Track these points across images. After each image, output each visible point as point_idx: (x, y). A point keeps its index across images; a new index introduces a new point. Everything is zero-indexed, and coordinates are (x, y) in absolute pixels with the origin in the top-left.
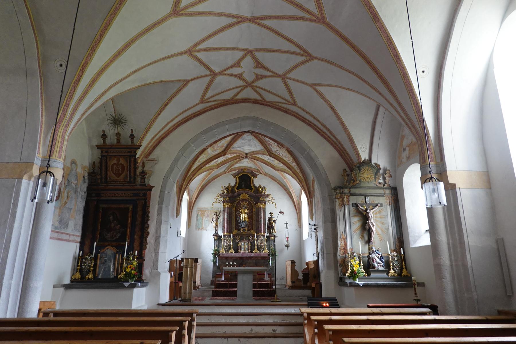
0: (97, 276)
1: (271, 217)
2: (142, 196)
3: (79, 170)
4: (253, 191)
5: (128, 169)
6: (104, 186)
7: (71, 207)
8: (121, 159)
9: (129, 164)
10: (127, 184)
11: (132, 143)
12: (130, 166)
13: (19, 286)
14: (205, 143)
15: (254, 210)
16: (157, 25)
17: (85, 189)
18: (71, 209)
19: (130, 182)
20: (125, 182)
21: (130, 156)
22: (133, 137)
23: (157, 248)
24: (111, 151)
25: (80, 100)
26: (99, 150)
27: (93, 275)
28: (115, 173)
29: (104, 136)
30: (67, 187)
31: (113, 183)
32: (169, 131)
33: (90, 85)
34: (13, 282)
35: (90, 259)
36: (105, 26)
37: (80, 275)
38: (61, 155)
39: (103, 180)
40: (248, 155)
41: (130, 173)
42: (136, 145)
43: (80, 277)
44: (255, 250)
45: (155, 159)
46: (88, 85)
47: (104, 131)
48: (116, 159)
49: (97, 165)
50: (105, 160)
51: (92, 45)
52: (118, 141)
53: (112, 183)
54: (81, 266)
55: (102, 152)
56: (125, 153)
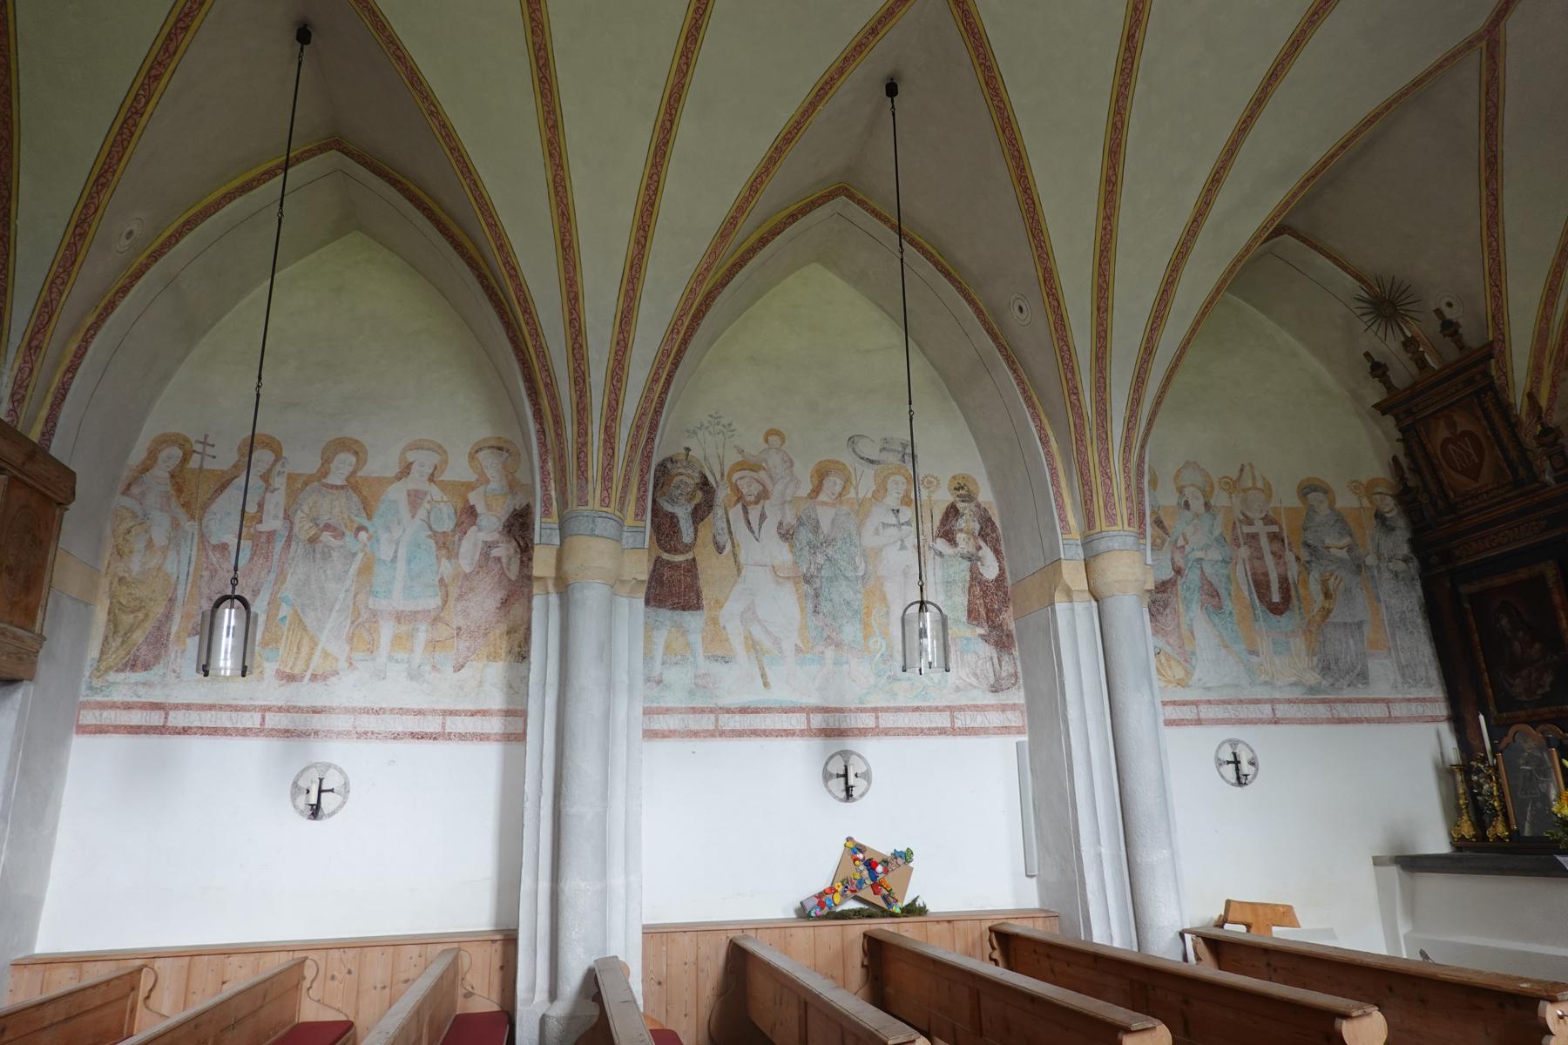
0: (1518, 831)
3: (1346, 501)
7: (1357, 620)
9: (1485, 423)
11: (1461, 348)
13: (1120, 860)
16: (1137, 35)
17: (1405, 549)
18: (1360, 625)
25: (1097, 359)
26: (1388, 416)
28: (1459, 468)
29: (1378, 370)
30: (1314, 565)
33: (1098, 309)
34: (1105, 851)
36: (1016, 163)
38: (1116, 515)
46: (1095, 312)
51: (1028, 227)
52: (1422, 364)
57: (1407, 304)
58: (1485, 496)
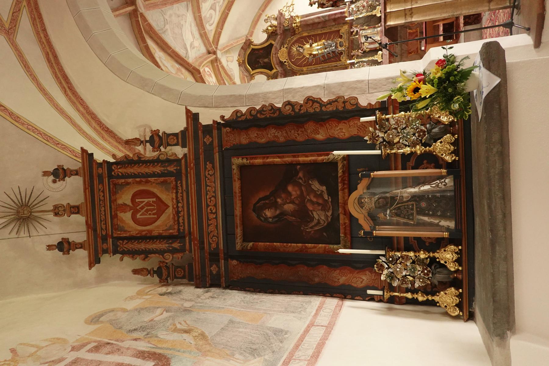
1: (317, 4)
2: (212, 138)
4: (273, 42)
5: (144, 180)
6: (190, 244)
8: (120, 202)
9: (130, 180)
10: (184, 183)
11: (76, 173)
12: (134, 176)
14: (157, 83)
15: (305, 34)
19: (178, 175)
20: (177, 186)
21: (110, 177)
22: (61, 171)
23: (356, 88)
24: (102, 229)
27: (446, 246)
31: (183, 220)
32: (84, 112)
35: (390, 265)
37: (444, 289)
39: (176, 245)
40: (210, 49)
41: (154, 175)
42: (83, 165)
43: (453, 289)
44: (376, 15)
45: (142, 134)
47: (50, 247)
48: (121, 215)
49: (138, 263)
50: (125, 241)
52: (75, 210)
53: (184, 223)
54: (414, 291)
55: (105, 251)
56: (103, 192)
57: (29, 199)
58: (180, 205)
